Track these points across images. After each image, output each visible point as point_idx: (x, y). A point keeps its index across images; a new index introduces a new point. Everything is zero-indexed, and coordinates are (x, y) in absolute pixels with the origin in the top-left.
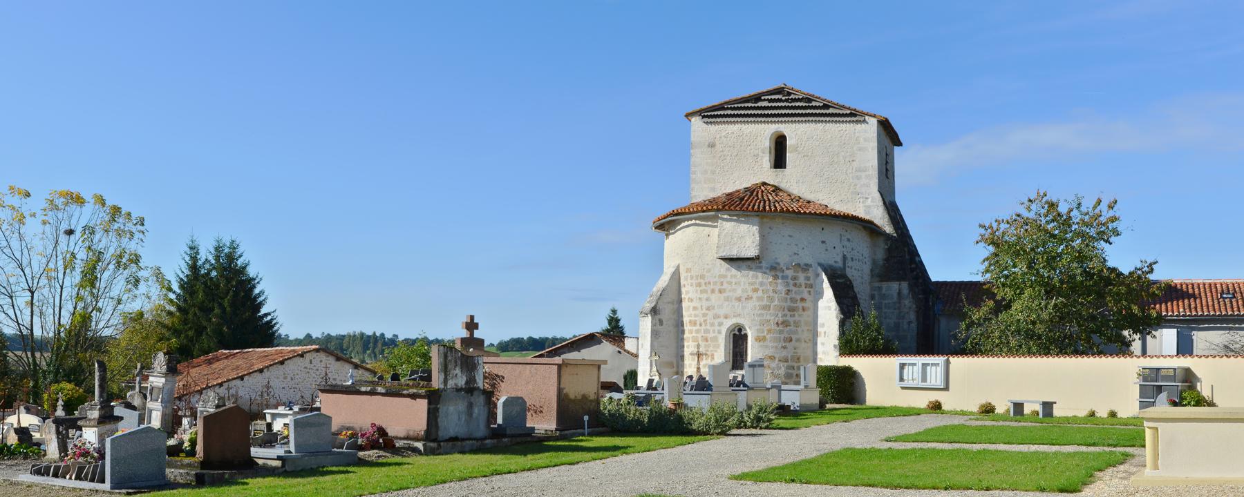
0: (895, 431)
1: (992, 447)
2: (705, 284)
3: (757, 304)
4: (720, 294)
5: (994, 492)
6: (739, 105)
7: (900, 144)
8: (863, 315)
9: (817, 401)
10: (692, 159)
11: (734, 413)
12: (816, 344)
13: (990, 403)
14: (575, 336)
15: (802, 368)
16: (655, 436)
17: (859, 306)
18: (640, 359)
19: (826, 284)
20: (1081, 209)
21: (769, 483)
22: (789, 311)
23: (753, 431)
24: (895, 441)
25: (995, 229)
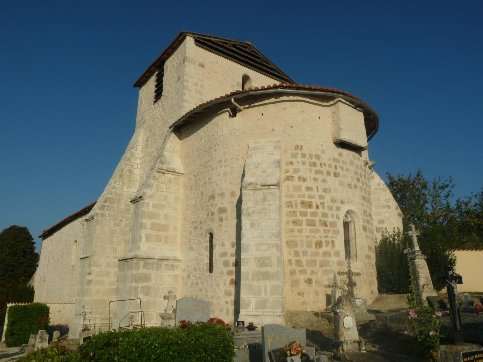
4: (335, 178)
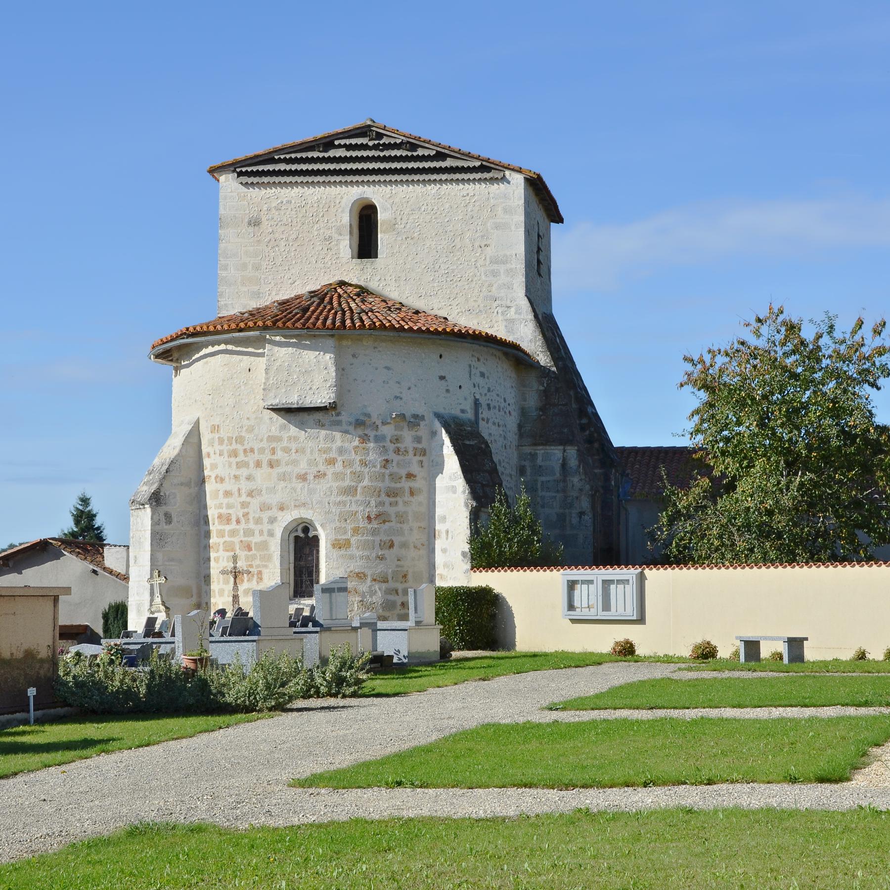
0: (563, 693)
1: (714, 713)
2: (245, 451)
3: (335, 485)
4: (270, 470)
5: (720, 786)
6: (299, 155)
7: (559, 219)
8: (507, 502)
9: (437, 648)
10: (222, 246)
11: (297, 672)
12: (432, 551)
13: (708, 643)
14: (12, 546)
15: (411, 592)
16: (159, 719)
17: (501, 485)
18: (132, 583)
19: (448, 449)
20: (835, 334)
21: (359, 790)
22: (389, 496)
23: (332, 702)
24: (564, 709)
25: (708, 364)
